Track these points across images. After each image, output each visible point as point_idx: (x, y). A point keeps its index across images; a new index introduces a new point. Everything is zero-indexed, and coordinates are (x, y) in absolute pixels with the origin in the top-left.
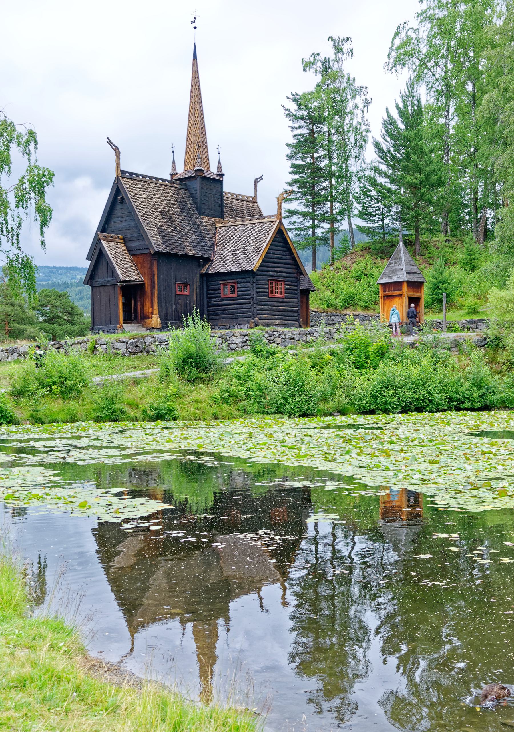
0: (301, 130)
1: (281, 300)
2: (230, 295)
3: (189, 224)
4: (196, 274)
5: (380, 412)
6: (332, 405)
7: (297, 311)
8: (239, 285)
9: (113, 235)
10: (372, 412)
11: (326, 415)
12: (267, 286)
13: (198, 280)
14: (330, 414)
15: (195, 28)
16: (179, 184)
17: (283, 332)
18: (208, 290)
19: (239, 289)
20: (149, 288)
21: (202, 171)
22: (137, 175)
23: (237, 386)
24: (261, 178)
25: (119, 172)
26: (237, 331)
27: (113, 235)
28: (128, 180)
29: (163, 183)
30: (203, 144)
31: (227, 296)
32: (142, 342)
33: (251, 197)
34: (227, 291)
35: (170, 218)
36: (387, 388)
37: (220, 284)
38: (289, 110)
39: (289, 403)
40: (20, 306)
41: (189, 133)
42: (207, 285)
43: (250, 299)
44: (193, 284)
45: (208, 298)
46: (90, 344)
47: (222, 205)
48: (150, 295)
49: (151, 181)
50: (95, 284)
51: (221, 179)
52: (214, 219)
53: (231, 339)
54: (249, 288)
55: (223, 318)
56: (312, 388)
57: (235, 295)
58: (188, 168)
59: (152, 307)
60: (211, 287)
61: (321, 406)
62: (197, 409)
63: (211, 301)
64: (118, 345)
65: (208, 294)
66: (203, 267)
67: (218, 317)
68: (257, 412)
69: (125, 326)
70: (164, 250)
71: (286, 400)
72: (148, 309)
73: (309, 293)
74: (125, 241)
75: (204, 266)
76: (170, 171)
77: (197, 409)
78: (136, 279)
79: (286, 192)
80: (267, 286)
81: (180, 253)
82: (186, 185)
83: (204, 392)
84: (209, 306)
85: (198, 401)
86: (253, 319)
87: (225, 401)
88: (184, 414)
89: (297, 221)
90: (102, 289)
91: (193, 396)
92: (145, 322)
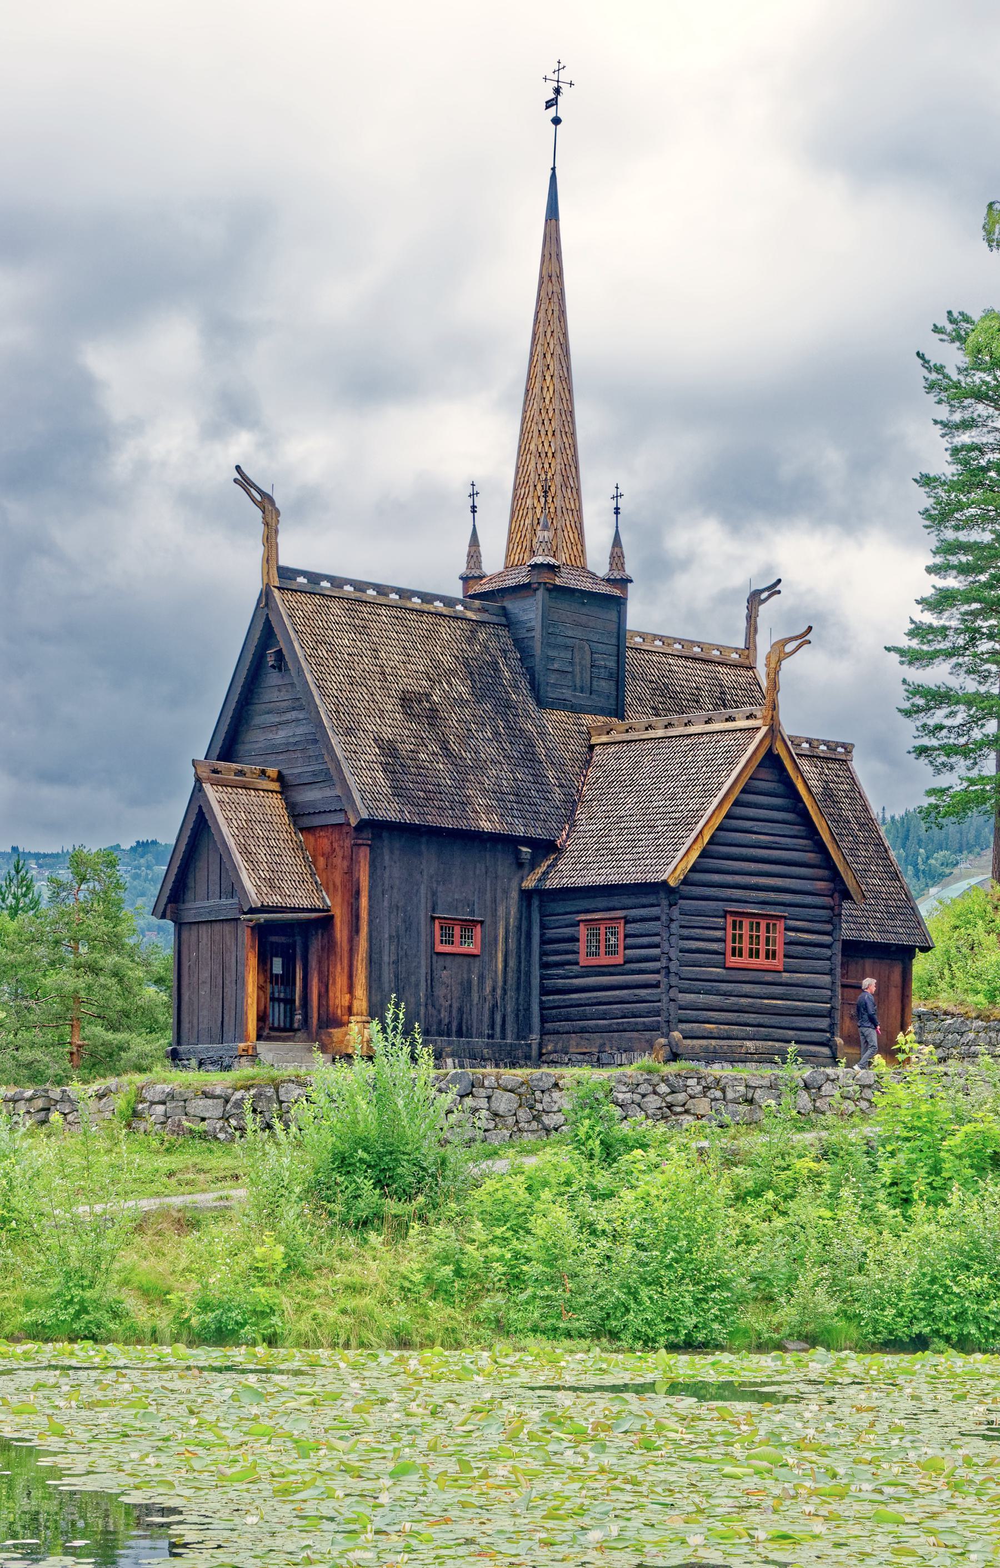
0: (974, 432)
1: (769, 977)
2: (605, 960)
3: (496, 733)
4: (506, 892)
5: (941, 1345)
6: (787, 1314)
7: (829, 1014)
8: (632, 928)
9: (246, 768)
10: (920, 1343)
11: (761, 1348)
12: (719, 934)
13: (513, 911)
14: (780, 1347)
15: (556, 121)
16: (483, 610)
17: (718, 1081)
18: (543, 942)
19: (630, 941)
20: (345, 933)
21: (551, 568)
22: (337, 582)
23: (484, 1246)
24: (773, 589)
25: (274, 572)
26: (569, 1074)
27: (246, 768)
28: (303, 598)
29: (426, 607)
30: (565, 485)
31: (594, 961)
32: (269, 1099)
33: (736, 650)
34: (597, 946)
35: (433, 716)
36: (968, 1268)
37: (577, 924)
38: (939, 369)
39: (640, 1304)
40: (115, 974)
41: (523, 450)
42: (543, 927)
43: (658, 972)
44: (495, 923)
45: (545, 966)
46: (120, 1102)
47: (618, 678)
48: (346, 955)
49: (382, 600)
50: (189, 917)
51: (617, 592)
52: (588, 720)
53: (546, 1098)
54: (656, 939)
55: (583, 1030)
56: (718, 1263)
57: (619, 959)
58: (516, 558)
59: (351, 989)
60: (551, 933)
61: (753, 1320)
62: (344, 1312)
63: (550, 977)
64: (199, 1106)
65: (543, 953)
66: (533, 868)
67: (566, 1025)
68: (535, 1330)
69: (262, 1047)
70: (408, 818)
71: (633, 1293)
72: (339, 998)
73: (912, 956)
74: (285, 784)
75: (534, 865)
76: (462, 568)
77: (344, 1312)
78: (306, 903)
79: (918, 631)
80: (719, 934)
81: (449, 824)
82: (504, 612)
83: (378, 1263)
84: (545, 991)
85: (355, 1289)
86: (667, 1036)
87: (438, 1290)
88: (304, 1325)
89: (948, 722)
90: (204, 929)
91: (345, 1273)
92: (330, 1035)
